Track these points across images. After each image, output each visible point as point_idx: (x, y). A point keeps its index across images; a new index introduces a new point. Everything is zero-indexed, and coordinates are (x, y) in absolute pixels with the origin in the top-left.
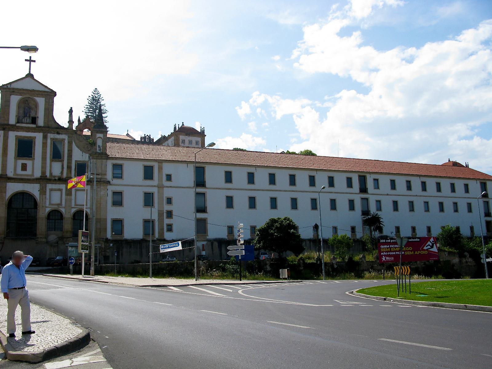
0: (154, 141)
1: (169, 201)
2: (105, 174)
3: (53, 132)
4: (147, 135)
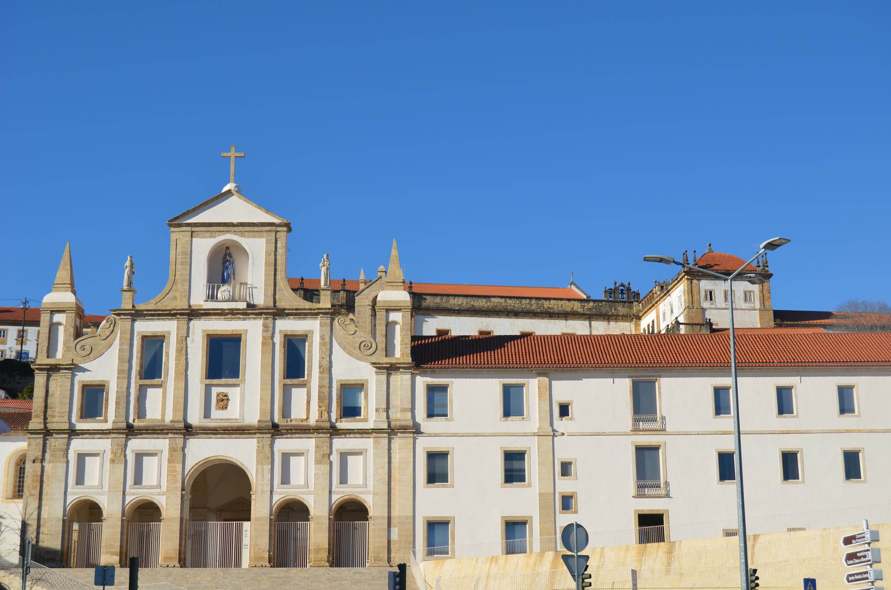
4: (622, 285)
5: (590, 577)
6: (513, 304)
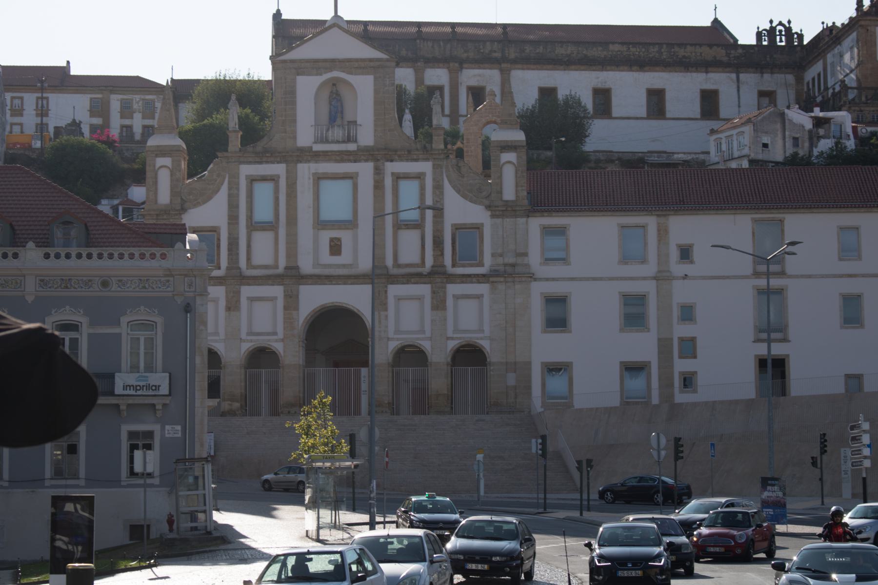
0: (805, 43)
1: (688, 313)
2: (525, 254)
4: (780, 24)
5: (682, 446)
6: (637, 53)
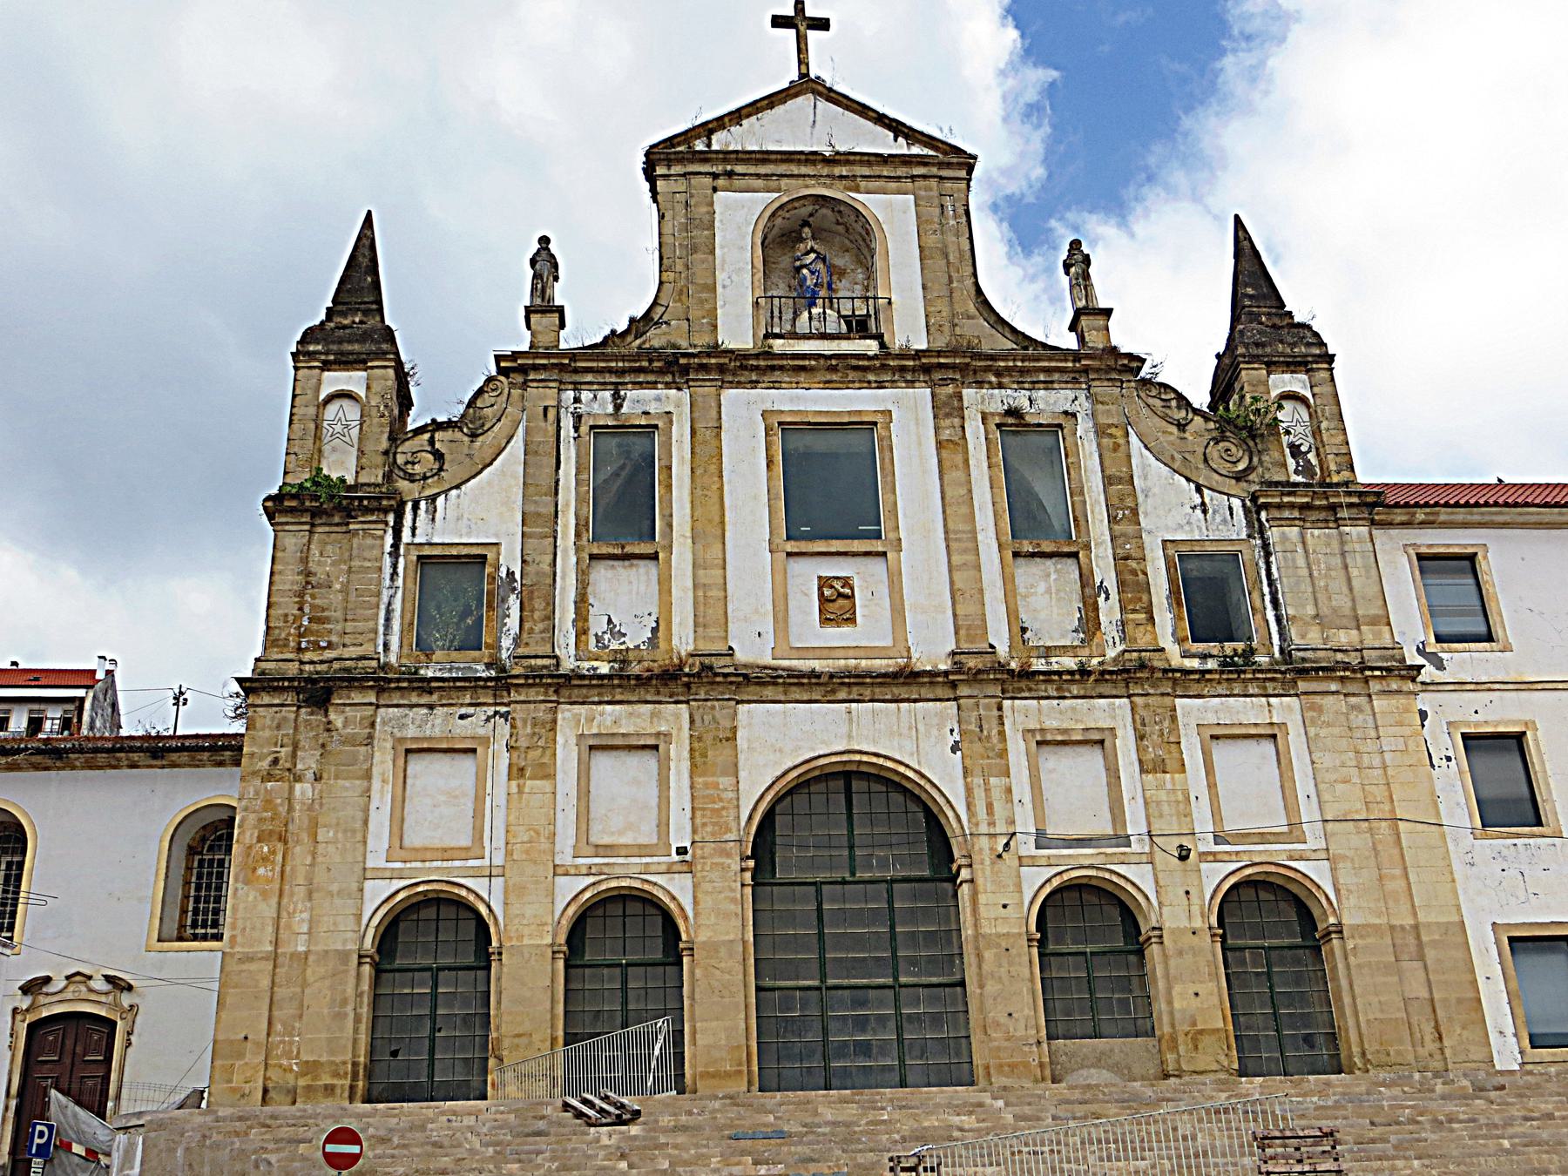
3: (993, 379)
